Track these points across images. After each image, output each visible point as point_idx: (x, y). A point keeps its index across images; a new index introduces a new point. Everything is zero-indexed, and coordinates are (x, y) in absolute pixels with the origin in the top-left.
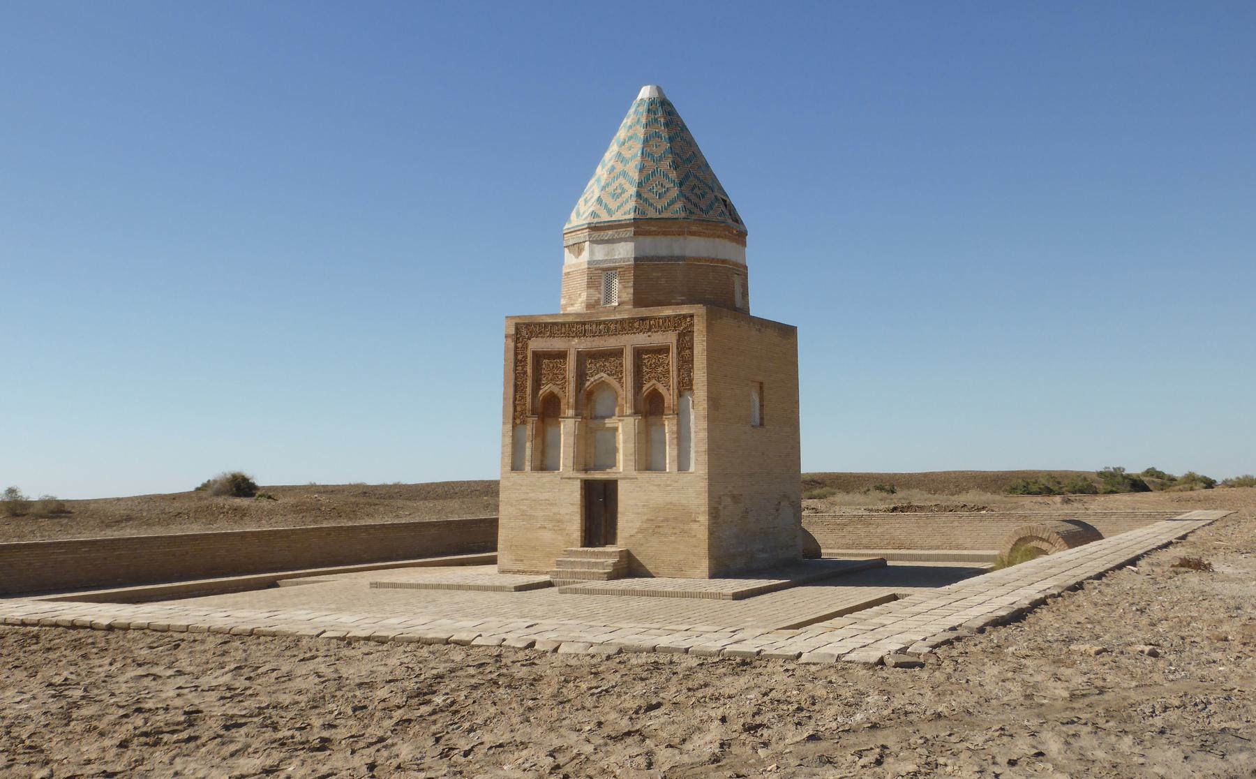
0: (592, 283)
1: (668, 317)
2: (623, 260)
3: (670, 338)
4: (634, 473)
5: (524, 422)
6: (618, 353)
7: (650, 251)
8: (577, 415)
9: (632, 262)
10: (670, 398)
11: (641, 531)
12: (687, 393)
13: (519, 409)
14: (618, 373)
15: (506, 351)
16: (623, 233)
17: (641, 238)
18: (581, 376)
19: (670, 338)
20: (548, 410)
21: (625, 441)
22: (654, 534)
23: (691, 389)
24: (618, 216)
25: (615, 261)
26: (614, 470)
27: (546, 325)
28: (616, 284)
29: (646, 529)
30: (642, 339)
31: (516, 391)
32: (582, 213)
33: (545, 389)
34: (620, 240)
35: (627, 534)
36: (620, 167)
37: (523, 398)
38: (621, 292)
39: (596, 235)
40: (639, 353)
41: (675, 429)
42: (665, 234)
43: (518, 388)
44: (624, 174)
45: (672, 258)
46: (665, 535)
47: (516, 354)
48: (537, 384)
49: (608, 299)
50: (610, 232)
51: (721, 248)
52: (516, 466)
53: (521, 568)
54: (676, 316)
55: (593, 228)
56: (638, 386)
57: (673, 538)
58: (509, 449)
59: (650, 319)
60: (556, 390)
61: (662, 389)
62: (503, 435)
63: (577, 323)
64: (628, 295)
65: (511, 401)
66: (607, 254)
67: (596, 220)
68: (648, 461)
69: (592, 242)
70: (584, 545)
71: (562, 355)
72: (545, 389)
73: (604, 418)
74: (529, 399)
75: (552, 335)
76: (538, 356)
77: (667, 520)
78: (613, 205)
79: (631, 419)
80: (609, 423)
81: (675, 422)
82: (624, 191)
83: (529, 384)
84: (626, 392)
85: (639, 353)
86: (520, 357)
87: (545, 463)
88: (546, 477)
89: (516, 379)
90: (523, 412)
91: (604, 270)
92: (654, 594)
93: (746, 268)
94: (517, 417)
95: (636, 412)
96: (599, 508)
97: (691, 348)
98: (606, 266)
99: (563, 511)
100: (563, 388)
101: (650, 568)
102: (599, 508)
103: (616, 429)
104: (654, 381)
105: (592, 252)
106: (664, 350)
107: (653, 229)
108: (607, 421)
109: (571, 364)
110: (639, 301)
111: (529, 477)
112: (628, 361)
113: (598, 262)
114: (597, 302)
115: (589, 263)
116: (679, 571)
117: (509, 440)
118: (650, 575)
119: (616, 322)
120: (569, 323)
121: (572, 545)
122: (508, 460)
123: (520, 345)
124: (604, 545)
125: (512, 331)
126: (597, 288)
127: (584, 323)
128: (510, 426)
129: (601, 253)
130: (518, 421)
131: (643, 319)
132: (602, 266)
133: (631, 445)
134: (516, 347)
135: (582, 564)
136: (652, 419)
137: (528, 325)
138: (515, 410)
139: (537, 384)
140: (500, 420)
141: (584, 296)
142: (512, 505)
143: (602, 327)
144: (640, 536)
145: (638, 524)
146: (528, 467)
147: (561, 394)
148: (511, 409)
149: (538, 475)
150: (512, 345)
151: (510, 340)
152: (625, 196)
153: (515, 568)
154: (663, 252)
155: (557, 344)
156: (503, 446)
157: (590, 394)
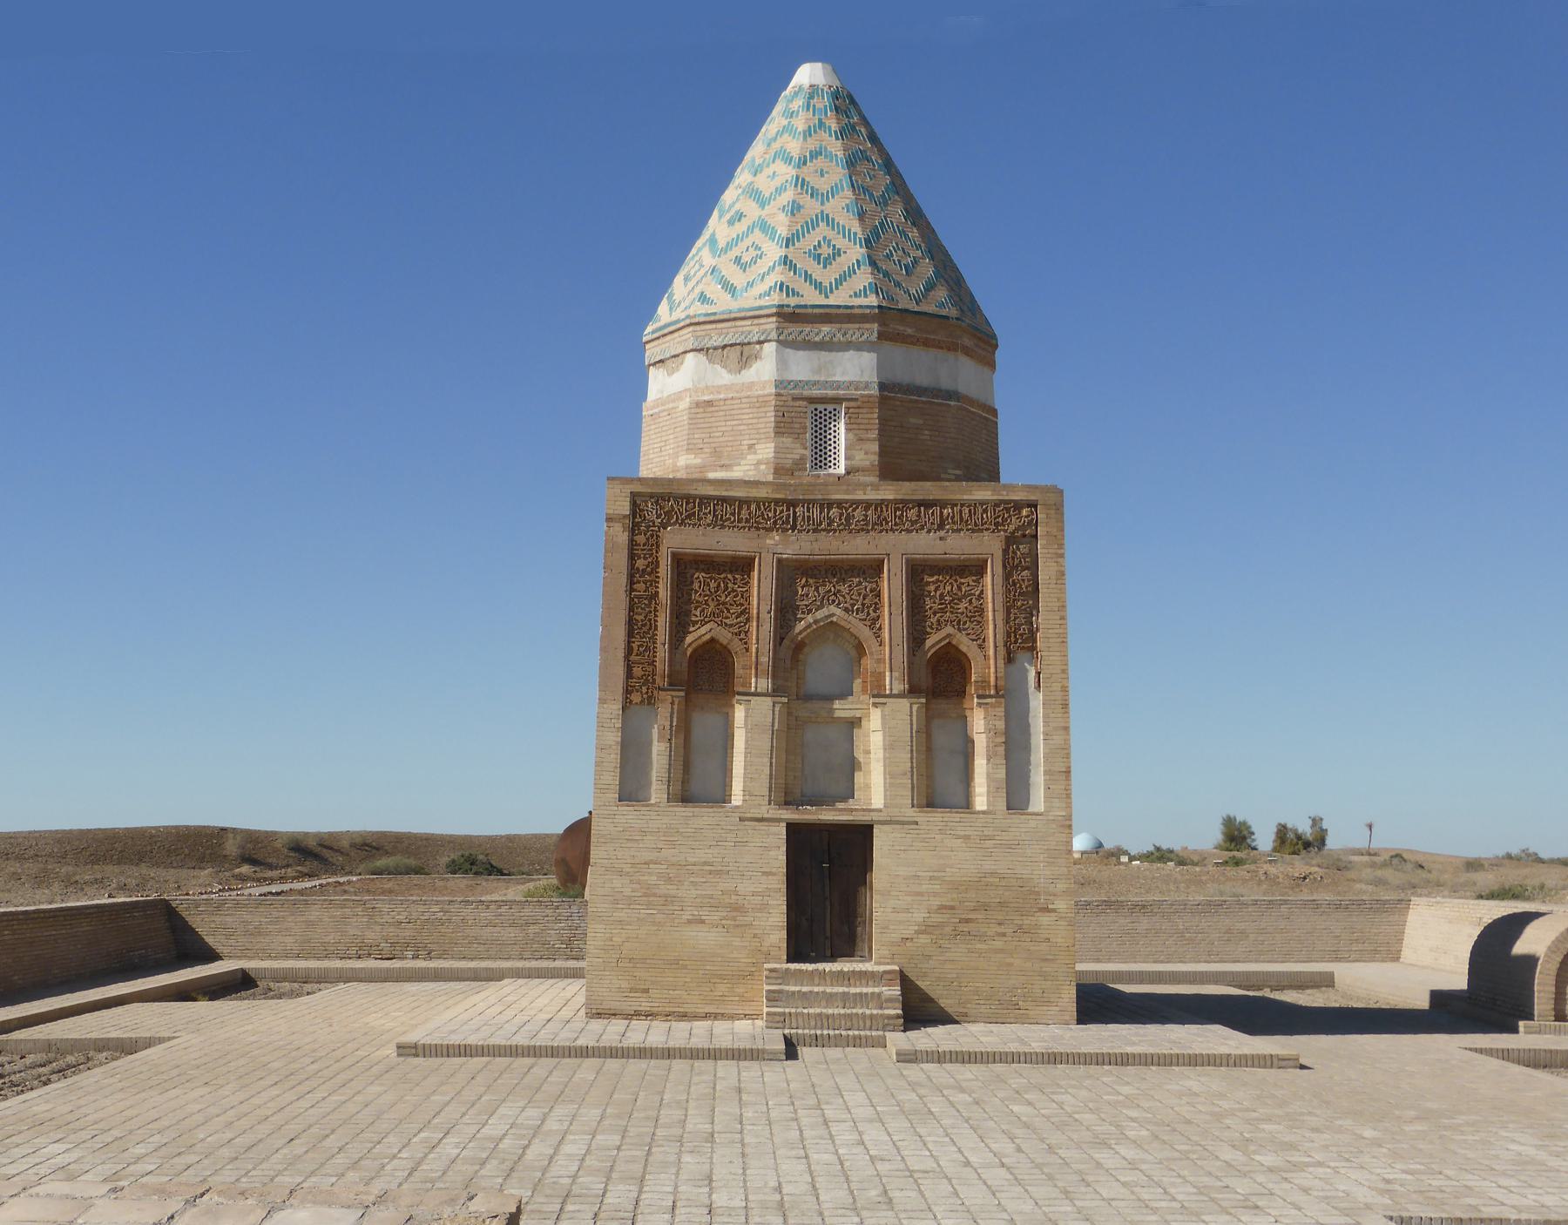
0: (784, 426)
1: (982, 503)
2: (856, 385)
3: (989, 545)
4: (912, 814)
5: (650, 701)
6: (873, 568)
7: (902, 375)
8: (776, 692)
9: (875, 391)
10: (985, 664)
11: (926, 929)
12: (1022, 657)
13: (637, 671)
14: (871, 610)
15: (610, 549)
16: (854, 332)
17: (887, 345)
18: (786, 612)
19: (989, 545)
20: (708, 677)
21: (889, 747)
22: (956, 934)
23: (1033, 649)
24: (839, 298)
25: (838, 385)
26: (851, 803)
27: (704, 500)
28: (841, 432)
29: (941, 925)
30: (926, 544)
31: (630, 634)
32: (692, 290)
33: (697, 635)
34: (847, 346)
35: (896, 936)
36: (812, 207)
37: (650, 649)
38: (846, 449)
39: (793, 330)
40: (918, 571)
41: (1001, 725)
42: (927, 343)
43: (637, 628)
44: (764, 226)
45: (936, 392)
46: (982, 938)
47: (632, 557)
48: (680, 624)
49: (821, 455)
50: (826, 329)
51: (960, 374)
52: (630, 791)
53: (645, 1006)
54: (997, 504)
55: (789, 316)
56: (916, 637)
57: (998, 944)
58: (614, 757)
59: (943, 504)
60: (724, 636)
61: (965, 644)
62: (601, 726)
63: (777, 502)
64: (869, 455)
65: (621, 654)
66: (819, 371)
67: (793, 301)
68: (937, 782)
69: (783, 343)
70: (791, 958)
71: (743, 566)
72: (697, 635)
73: (830, 698)
74: (662, 652)
75: (719, 523)
76: (684, 565)
77: (985, 907)
78: (738, 278)
79: (904, 703)
80: (842, 709)
81: (1000, 711)
82: (837, 253)
83: (663, 621)
84: (888, 652)
85: (918, 571)
86: (640, 564)
87: (696, 785)
88: (703, 817)
89: (631, 609)
90: (648, 679)
91: (812, 400)
92: (939, 1057)
93: (994, 412)
94: (636, 684)
95: (913, 691)
96: (827, 884)
97: (1034, 567)
98: (816, 392)
99: (745, 887)
100: (742, 634)
101: (947, 1003)
102: (827, 884)
103: (854, 723)
104: (949, 629)
105: (782, 363)
106: (976, 568)
107: (910, 331)
108: (837, 704)
109: (761, 589)
110: (889, 470)
111: (657, 811)
112: (892, 586)
113: (797, 384)
114: (799, 464)
115: (779, 384)
116: (1008, 1010)
117: (613, 738)
118: (944, 1018)
119: (867, 505)
120: (758, 502)
121: (768, 957)
122: (612, 779)
123: (641, 539)
124: (833, 958)
125: (625, 509)
126: (798, 436)
127: (792, 504)
128: (616, 707)
129: (803, 367)
130: (636, 698)
131: (927, 504)
132: (806, 393)
133: (765, 742)
134: (632, 544)
135: (830, 999)
136: (942, 705)
137: (659, 499)
138: (629, 674)
139: (680, 624)
140: (595, 693)
141: (766, 450)
142: (621, 873)
143: (834, 511)
144: (924, 939)
145: (919, 916)
146: (657, 792)
147: (736, 646)
148: (620, 671)
149: (682, 811)
150: (623, 538)
151: (618, 527)
152: (845, 262)
153: (629, 1006)
154: (923, 380)
155: (731, 542)
156: (601, 748)
157: (799, 647)
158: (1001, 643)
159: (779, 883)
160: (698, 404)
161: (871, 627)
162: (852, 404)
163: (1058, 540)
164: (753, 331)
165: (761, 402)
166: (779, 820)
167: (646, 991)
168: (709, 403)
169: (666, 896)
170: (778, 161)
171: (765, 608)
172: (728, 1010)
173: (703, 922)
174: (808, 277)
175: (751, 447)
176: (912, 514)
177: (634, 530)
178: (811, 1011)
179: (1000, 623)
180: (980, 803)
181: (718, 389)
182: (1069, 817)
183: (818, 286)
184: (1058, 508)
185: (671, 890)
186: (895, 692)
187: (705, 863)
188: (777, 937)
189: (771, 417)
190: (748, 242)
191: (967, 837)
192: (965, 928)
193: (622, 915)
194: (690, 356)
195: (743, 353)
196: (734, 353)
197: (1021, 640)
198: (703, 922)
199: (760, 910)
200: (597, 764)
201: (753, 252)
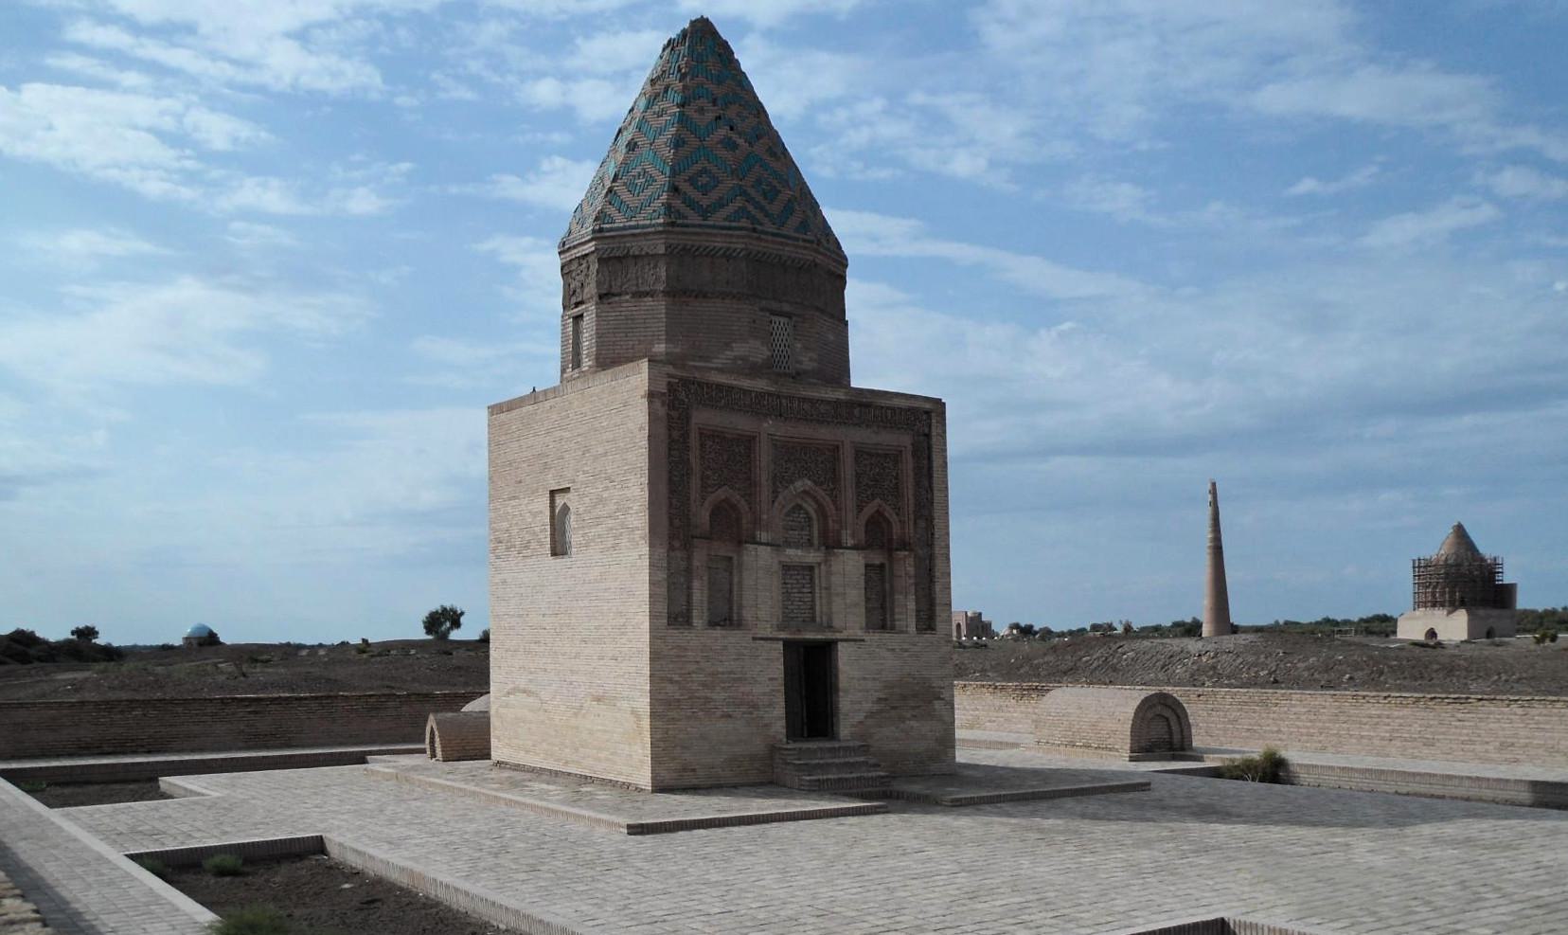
3: (905, 440)
61: (889, 512)
144: (870, 722)
145: (867, 706)
147: (743, 505)
150: (662, 411)
151: (658, 404)
177: (671, 406)
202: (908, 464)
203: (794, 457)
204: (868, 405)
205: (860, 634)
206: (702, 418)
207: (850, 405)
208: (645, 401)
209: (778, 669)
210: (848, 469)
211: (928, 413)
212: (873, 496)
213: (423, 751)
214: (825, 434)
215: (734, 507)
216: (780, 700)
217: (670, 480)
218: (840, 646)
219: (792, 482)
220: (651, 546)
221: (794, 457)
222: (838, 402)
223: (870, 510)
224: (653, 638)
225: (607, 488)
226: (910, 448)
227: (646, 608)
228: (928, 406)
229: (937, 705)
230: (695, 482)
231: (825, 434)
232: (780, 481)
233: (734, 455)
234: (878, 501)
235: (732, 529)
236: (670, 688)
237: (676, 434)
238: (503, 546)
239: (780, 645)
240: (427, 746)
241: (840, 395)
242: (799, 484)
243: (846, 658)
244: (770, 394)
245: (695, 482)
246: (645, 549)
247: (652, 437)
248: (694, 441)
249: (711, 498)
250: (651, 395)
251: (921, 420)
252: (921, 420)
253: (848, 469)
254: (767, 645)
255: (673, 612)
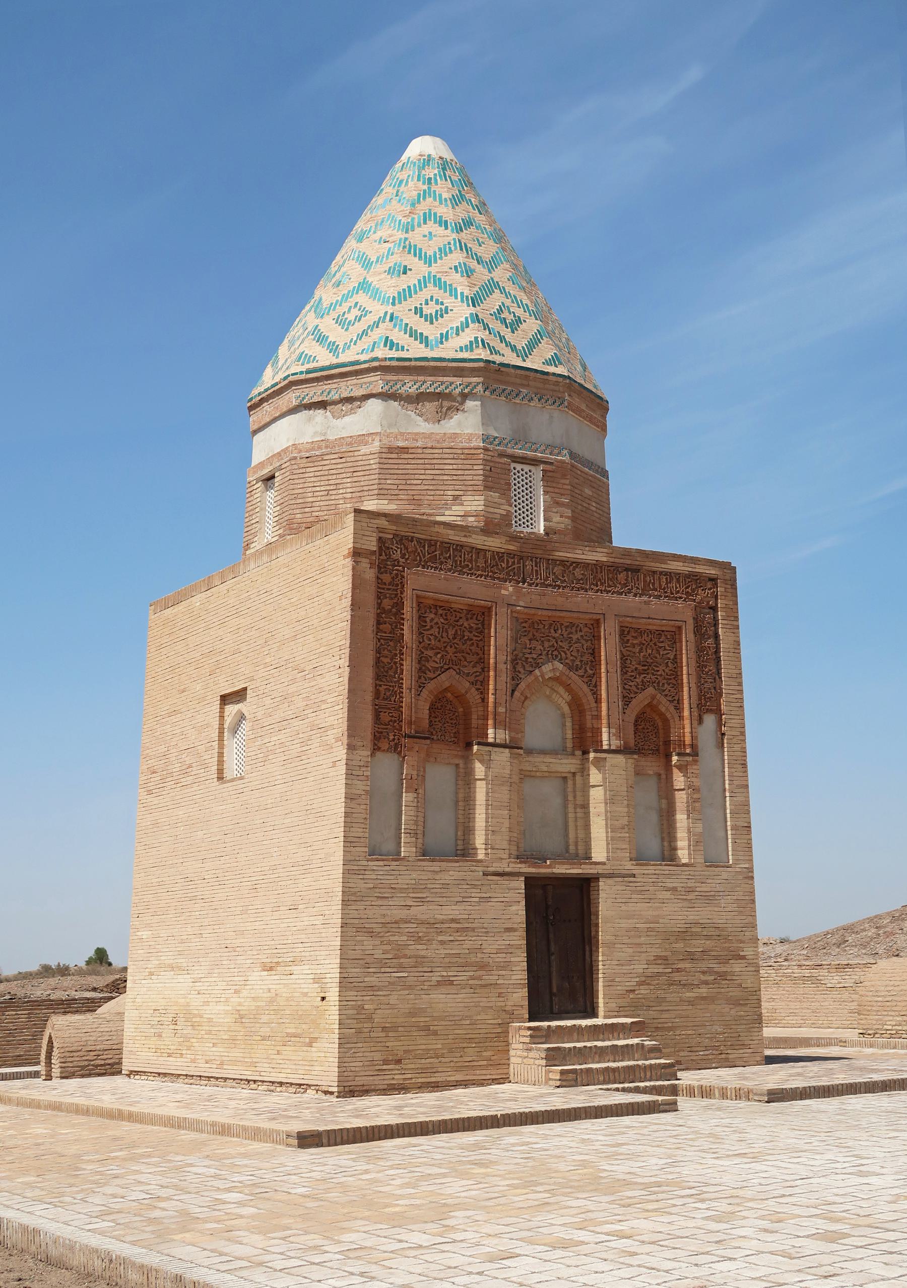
3: (681, 611)
4: (629, 866)
21: (610, 801)
47: (379, 596)
57: (703, 991)
60: (464, 685)
61: (665, 706)
75: (460, 568)
89: (378, 651)
99: (491, 945)
125: (373, 546)
142: (371, 933)
144: (644, 991)
145: (639, 968)
147: (473, 696)
150: (370, 574)
151: (365, 563)
158: (694, 706)
159: (519, 939)
160: (391, 450)
161: (588, 684)
162: (548, 467)
163: (733, 615)
164: (457, 384)
165: (468, 455)
166: (518, 874)
167: (399, 1062)
168: (404, 450)
169: (416, 957)
170: (430, 223)
171: (502, 658)
172: (478, 1075)
173: (451, 983)
174: (502, 339)
175: (456, 498)
176: (622, 577)
177: (381, 568)
178: (647, 1063)
179: (693, 686)
180: (683, 855)
181: (416, 436)
182: (751, 869)
183: (514, 348)
184: (732, 583)
185: (420, 949)
186: (613, 747)
187: (453, 921)
188: (520, 997)
189: (479, 470)
190: (351, 302)
191: (674, 889)
192: (677, 977)
193: (371, 980)
194: (372, 401)
195: (446, 403)
196: (430, 407)
197: (710, 701)
198: (451, 983)
199: (503, 968)
200: (347, 815)
201: (356, 312)
202: (688, 639)
203: (540, 637)
204: (636, 570)
205: (629, 866)
206: (420, 581)
207: (613, 569)
208: (349, 562)
209: (518, 912)
210: (609, 648)
211: (714, 580)
212: (644, 686)
213: (36, 1075)
214: (583, 602)
215: (459, 697)
216: (520, 960)
217: (378, 661)
218: (602, 883)
219: (538, 666)
220: (351, 747)
221: (540, 637)
222: (597, 567)
223: (640, 701)
224: (347, 873)
225: (294, 681)
226: (691, 622)
227: (340, 832)
228: (712, 572)
229: (737, 967)
230: (408, 666)
231: (583, 602)
232: (521, 664)
233: (459, 632)
234: (650, 690)
235: (453, 728)
236: (368, 944)
237: (387, 604)
238: (157, 778)
239: (520, 884)
240: (41, 1068)
241: (598, 556)
242: (547, 668)
243: (609, 904)
244: (510, 554)
245: (408, 666)
246: (341, 752)
247: (355, 605)
248: (409, 610)
249: (431, 685)
250: (356, 553)
251: (707, 590)
252: (707, 590)
253: (609, 648)
254: (504, 882)
255: (370, 843)
